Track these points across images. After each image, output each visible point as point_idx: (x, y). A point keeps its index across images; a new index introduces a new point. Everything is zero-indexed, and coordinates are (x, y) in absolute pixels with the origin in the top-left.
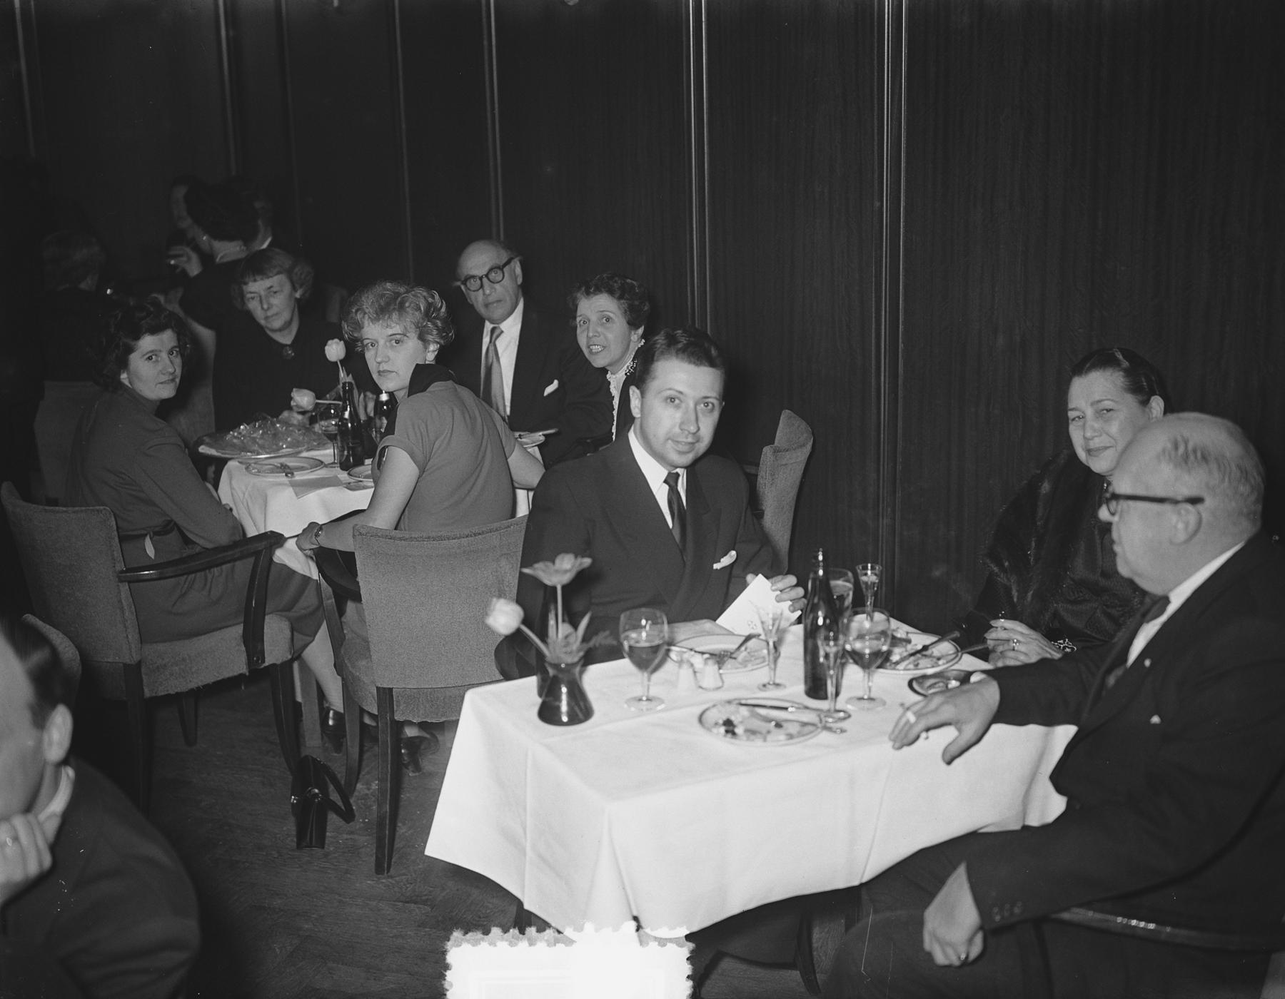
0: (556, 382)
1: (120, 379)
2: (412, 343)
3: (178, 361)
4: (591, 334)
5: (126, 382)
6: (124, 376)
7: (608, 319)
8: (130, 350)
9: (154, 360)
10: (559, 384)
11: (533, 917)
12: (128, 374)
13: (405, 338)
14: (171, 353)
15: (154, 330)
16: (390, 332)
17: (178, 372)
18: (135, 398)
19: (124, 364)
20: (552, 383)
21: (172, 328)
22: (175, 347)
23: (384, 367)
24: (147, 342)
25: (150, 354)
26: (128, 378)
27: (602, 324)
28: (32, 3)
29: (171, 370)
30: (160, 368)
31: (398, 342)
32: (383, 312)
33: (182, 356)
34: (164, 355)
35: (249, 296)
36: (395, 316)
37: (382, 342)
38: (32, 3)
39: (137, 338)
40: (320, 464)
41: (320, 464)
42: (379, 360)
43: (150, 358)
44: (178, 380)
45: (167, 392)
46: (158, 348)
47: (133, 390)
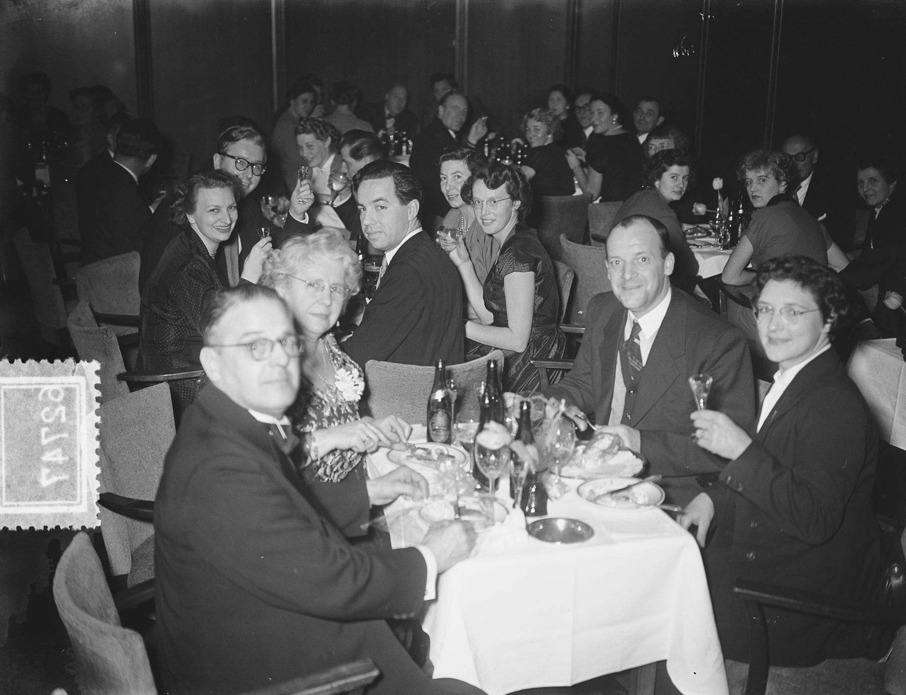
0: (825, 215)
1: (654, 183)
2: (771, 181)
3: (686, 183)
4: (865, 190)
5: (657, 186)
6: (657, 183)
7: (875, 180)
8: (665, 170)
9: (675, 178)
10: (827, 216)
11: (619, 680)
12: (660, 182)
13: (768, 179)
14: (684, 178)
15: (681, 164)
16: (759, 175)
17: (685, 189)
18: (658, 195)
19: (659, 177)
20: (823, 215)
21: (689, 166)
22: (687, 176)
23: (755, 194)
24: (675, 169)
25: (674, 175)
26: (659, 184)
27: (872, 183)
28: (783, 1)
29: (681, 186)
30: (677, 183)
31: (764, 181)
32: (756, 165)
33: (689, 182)
34: (680, 178)
35: (651, 146)
36: (762, 167)
37: (755, 181)
38: (783, 1)
39: (671, 165)
40: (709, 244)
41: (709, 244)
42: (752, 190)
43: (673, 177)
44: (683, 193)
45: (676, 197)
46: (679, 173)
47: (659, 191)
